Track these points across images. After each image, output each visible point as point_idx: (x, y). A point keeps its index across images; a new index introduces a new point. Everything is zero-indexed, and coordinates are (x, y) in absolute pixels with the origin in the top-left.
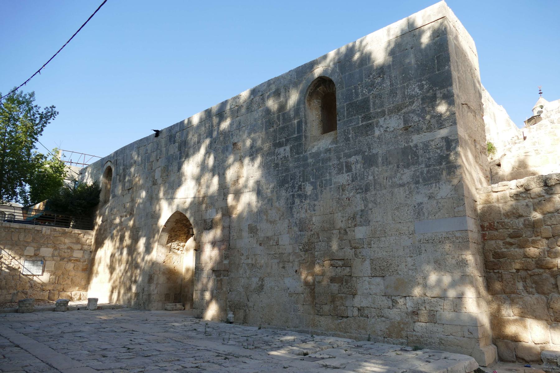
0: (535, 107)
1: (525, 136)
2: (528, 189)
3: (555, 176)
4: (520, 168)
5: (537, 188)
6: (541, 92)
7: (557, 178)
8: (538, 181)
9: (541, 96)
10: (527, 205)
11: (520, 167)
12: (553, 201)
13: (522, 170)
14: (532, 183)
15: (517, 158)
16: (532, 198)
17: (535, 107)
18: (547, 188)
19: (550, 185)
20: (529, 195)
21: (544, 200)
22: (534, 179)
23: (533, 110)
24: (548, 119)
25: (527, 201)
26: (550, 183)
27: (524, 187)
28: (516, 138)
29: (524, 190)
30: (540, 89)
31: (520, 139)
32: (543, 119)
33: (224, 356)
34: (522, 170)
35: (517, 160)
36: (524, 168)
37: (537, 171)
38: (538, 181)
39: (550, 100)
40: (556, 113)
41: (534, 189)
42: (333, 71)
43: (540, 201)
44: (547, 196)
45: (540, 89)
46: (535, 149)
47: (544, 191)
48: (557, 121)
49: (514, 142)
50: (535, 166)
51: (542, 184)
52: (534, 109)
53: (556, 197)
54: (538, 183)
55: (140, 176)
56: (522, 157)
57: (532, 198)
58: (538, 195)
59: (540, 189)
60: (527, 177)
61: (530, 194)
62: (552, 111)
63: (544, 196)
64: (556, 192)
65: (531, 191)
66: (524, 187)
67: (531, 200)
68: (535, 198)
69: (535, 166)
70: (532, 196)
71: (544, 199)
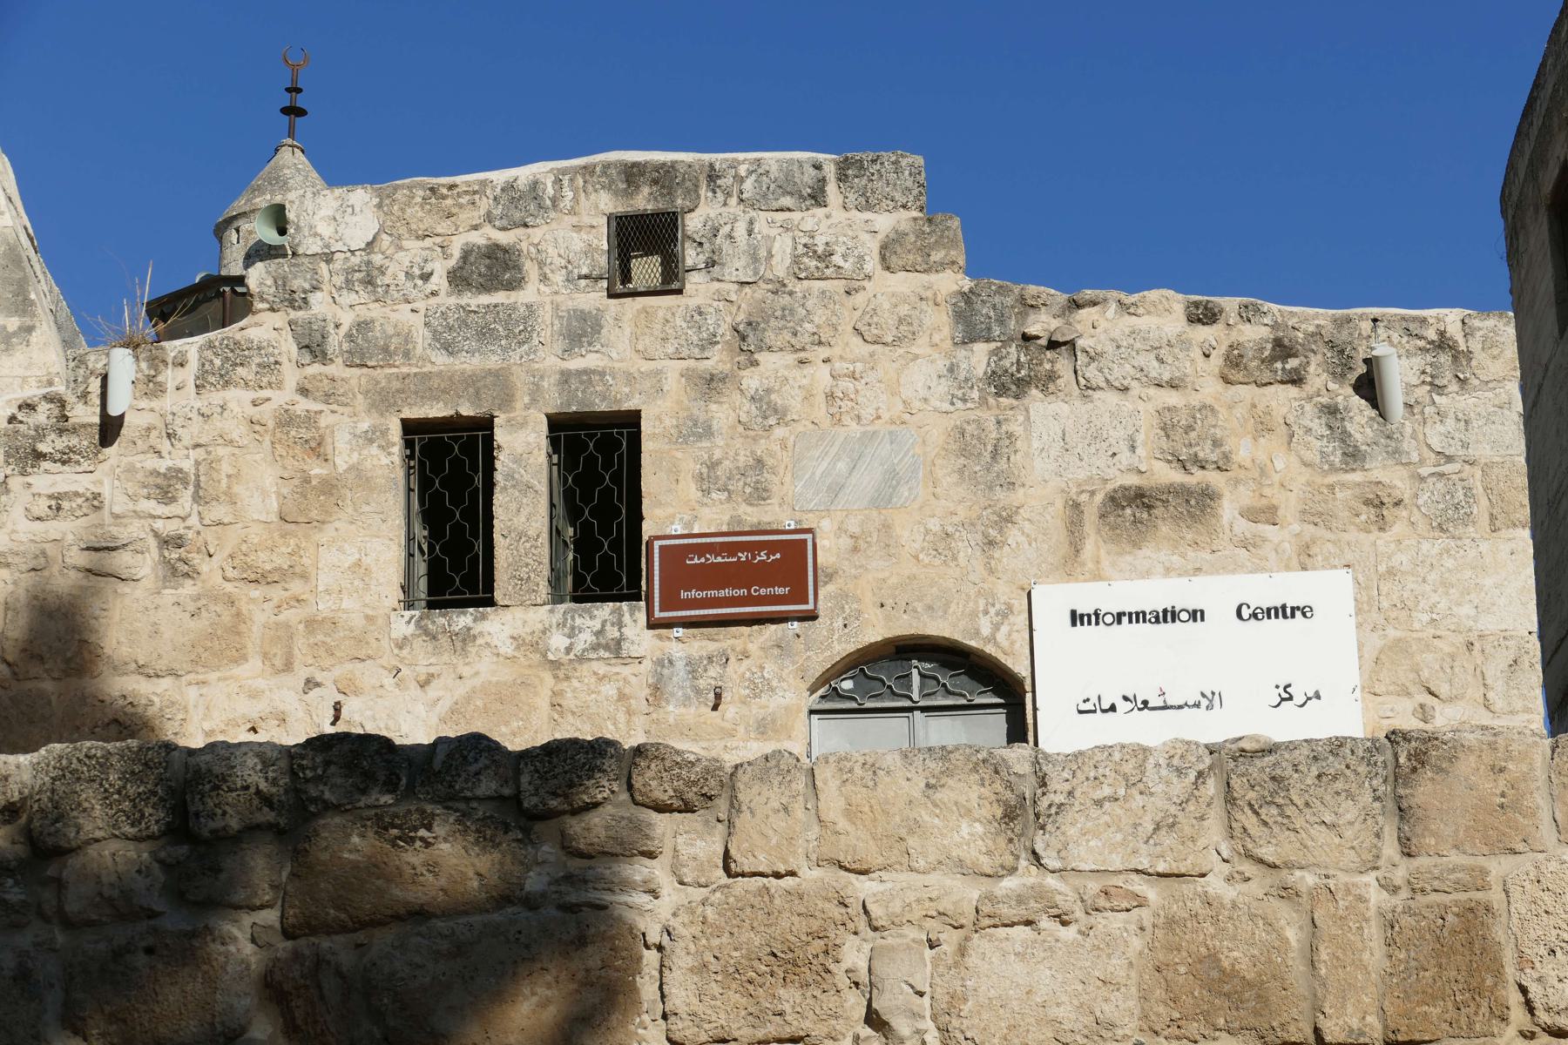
0: (240, 205)
1: (114, 411)
2: (50, 841)
3: (252, 761)
4: (35, 669)
5: (114, 845)
6: (301, 101)
7: (263, 786)
8: (131, 790)
9: (291, 134)
10: (23, 976)
11: (41, 659)
12: (208, 961)
13: (48, 686)
14: (89, 795)
15: (27, 580)
16: (68, 923)
17: (240, 205)
18: (183, 850)
19: (205, 833)
20: (48, 895)
21: (149, 951)
22: (104, 765)
23: (220, 230)
24: (293, 314)
25: (24, 940)
26: (212, 816)
27: (23, 819)
28: (43, 414)
29: (21, 850)
30: (294, 79)
31: (74, 430)
32: (259, 305)
33: (1151, 892)
34: (48, 686)
35: (21, 592)
36: (67, 673)
37: (151, 711)
38: (131, 790)
39: (336, 173)
40: (349, 286)
41: (92, 851)
42: (250, 773)
43: (118, 954)
44: (174, 921)
45: (294, 79)
46: (169, 528)
47: (162, 878)
48: (346, 346)
49: (26, 443)
50: (141, 669)
51: (155, 817)
52: (230, 220)
53: (235, 932)
54: (126, 805)
55: (145, 1002)
56: (63, 582)
57: (68, 923)
58: (110, 901)
59: (132, 854)
60: (58, 746)
61: (59, 884)
62: (328, 258)
63: (152, 915)
64: (240, 896)
65: (74, 862)
66: (23, 819)
67: (61, 938)
68: (90, 924)
69: (141, 669)
70: (72, 907)
71: (150, 941)
